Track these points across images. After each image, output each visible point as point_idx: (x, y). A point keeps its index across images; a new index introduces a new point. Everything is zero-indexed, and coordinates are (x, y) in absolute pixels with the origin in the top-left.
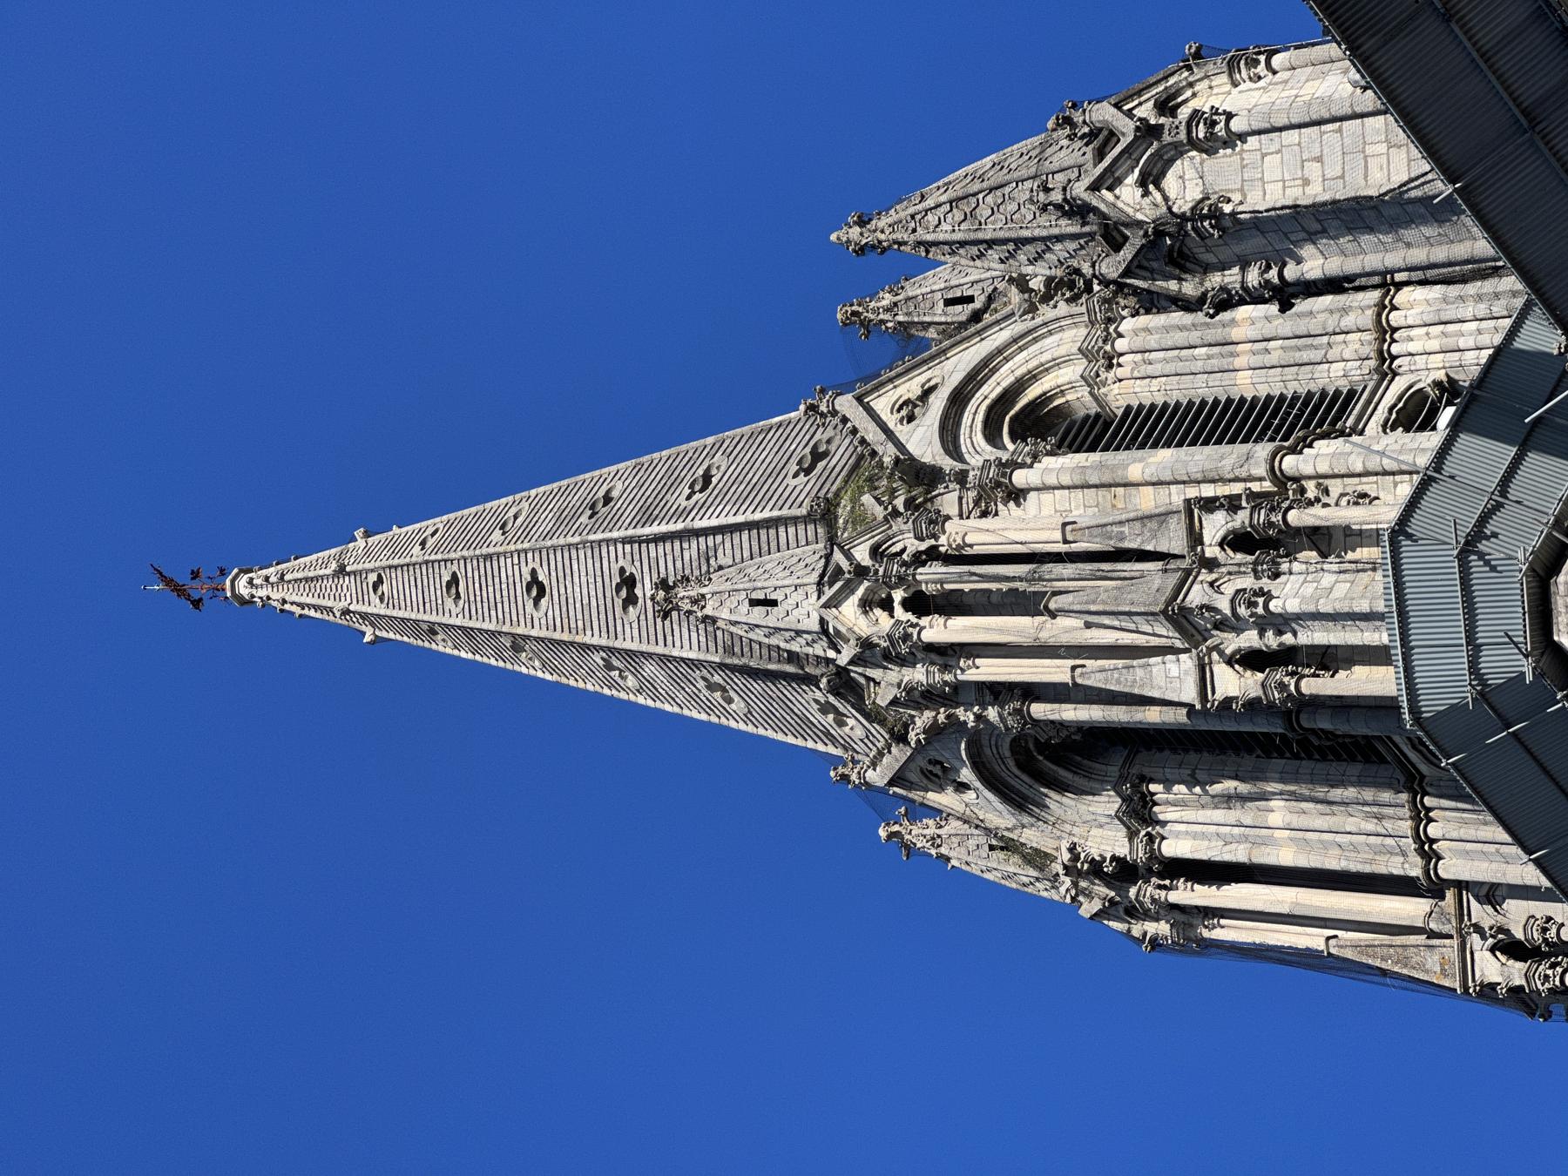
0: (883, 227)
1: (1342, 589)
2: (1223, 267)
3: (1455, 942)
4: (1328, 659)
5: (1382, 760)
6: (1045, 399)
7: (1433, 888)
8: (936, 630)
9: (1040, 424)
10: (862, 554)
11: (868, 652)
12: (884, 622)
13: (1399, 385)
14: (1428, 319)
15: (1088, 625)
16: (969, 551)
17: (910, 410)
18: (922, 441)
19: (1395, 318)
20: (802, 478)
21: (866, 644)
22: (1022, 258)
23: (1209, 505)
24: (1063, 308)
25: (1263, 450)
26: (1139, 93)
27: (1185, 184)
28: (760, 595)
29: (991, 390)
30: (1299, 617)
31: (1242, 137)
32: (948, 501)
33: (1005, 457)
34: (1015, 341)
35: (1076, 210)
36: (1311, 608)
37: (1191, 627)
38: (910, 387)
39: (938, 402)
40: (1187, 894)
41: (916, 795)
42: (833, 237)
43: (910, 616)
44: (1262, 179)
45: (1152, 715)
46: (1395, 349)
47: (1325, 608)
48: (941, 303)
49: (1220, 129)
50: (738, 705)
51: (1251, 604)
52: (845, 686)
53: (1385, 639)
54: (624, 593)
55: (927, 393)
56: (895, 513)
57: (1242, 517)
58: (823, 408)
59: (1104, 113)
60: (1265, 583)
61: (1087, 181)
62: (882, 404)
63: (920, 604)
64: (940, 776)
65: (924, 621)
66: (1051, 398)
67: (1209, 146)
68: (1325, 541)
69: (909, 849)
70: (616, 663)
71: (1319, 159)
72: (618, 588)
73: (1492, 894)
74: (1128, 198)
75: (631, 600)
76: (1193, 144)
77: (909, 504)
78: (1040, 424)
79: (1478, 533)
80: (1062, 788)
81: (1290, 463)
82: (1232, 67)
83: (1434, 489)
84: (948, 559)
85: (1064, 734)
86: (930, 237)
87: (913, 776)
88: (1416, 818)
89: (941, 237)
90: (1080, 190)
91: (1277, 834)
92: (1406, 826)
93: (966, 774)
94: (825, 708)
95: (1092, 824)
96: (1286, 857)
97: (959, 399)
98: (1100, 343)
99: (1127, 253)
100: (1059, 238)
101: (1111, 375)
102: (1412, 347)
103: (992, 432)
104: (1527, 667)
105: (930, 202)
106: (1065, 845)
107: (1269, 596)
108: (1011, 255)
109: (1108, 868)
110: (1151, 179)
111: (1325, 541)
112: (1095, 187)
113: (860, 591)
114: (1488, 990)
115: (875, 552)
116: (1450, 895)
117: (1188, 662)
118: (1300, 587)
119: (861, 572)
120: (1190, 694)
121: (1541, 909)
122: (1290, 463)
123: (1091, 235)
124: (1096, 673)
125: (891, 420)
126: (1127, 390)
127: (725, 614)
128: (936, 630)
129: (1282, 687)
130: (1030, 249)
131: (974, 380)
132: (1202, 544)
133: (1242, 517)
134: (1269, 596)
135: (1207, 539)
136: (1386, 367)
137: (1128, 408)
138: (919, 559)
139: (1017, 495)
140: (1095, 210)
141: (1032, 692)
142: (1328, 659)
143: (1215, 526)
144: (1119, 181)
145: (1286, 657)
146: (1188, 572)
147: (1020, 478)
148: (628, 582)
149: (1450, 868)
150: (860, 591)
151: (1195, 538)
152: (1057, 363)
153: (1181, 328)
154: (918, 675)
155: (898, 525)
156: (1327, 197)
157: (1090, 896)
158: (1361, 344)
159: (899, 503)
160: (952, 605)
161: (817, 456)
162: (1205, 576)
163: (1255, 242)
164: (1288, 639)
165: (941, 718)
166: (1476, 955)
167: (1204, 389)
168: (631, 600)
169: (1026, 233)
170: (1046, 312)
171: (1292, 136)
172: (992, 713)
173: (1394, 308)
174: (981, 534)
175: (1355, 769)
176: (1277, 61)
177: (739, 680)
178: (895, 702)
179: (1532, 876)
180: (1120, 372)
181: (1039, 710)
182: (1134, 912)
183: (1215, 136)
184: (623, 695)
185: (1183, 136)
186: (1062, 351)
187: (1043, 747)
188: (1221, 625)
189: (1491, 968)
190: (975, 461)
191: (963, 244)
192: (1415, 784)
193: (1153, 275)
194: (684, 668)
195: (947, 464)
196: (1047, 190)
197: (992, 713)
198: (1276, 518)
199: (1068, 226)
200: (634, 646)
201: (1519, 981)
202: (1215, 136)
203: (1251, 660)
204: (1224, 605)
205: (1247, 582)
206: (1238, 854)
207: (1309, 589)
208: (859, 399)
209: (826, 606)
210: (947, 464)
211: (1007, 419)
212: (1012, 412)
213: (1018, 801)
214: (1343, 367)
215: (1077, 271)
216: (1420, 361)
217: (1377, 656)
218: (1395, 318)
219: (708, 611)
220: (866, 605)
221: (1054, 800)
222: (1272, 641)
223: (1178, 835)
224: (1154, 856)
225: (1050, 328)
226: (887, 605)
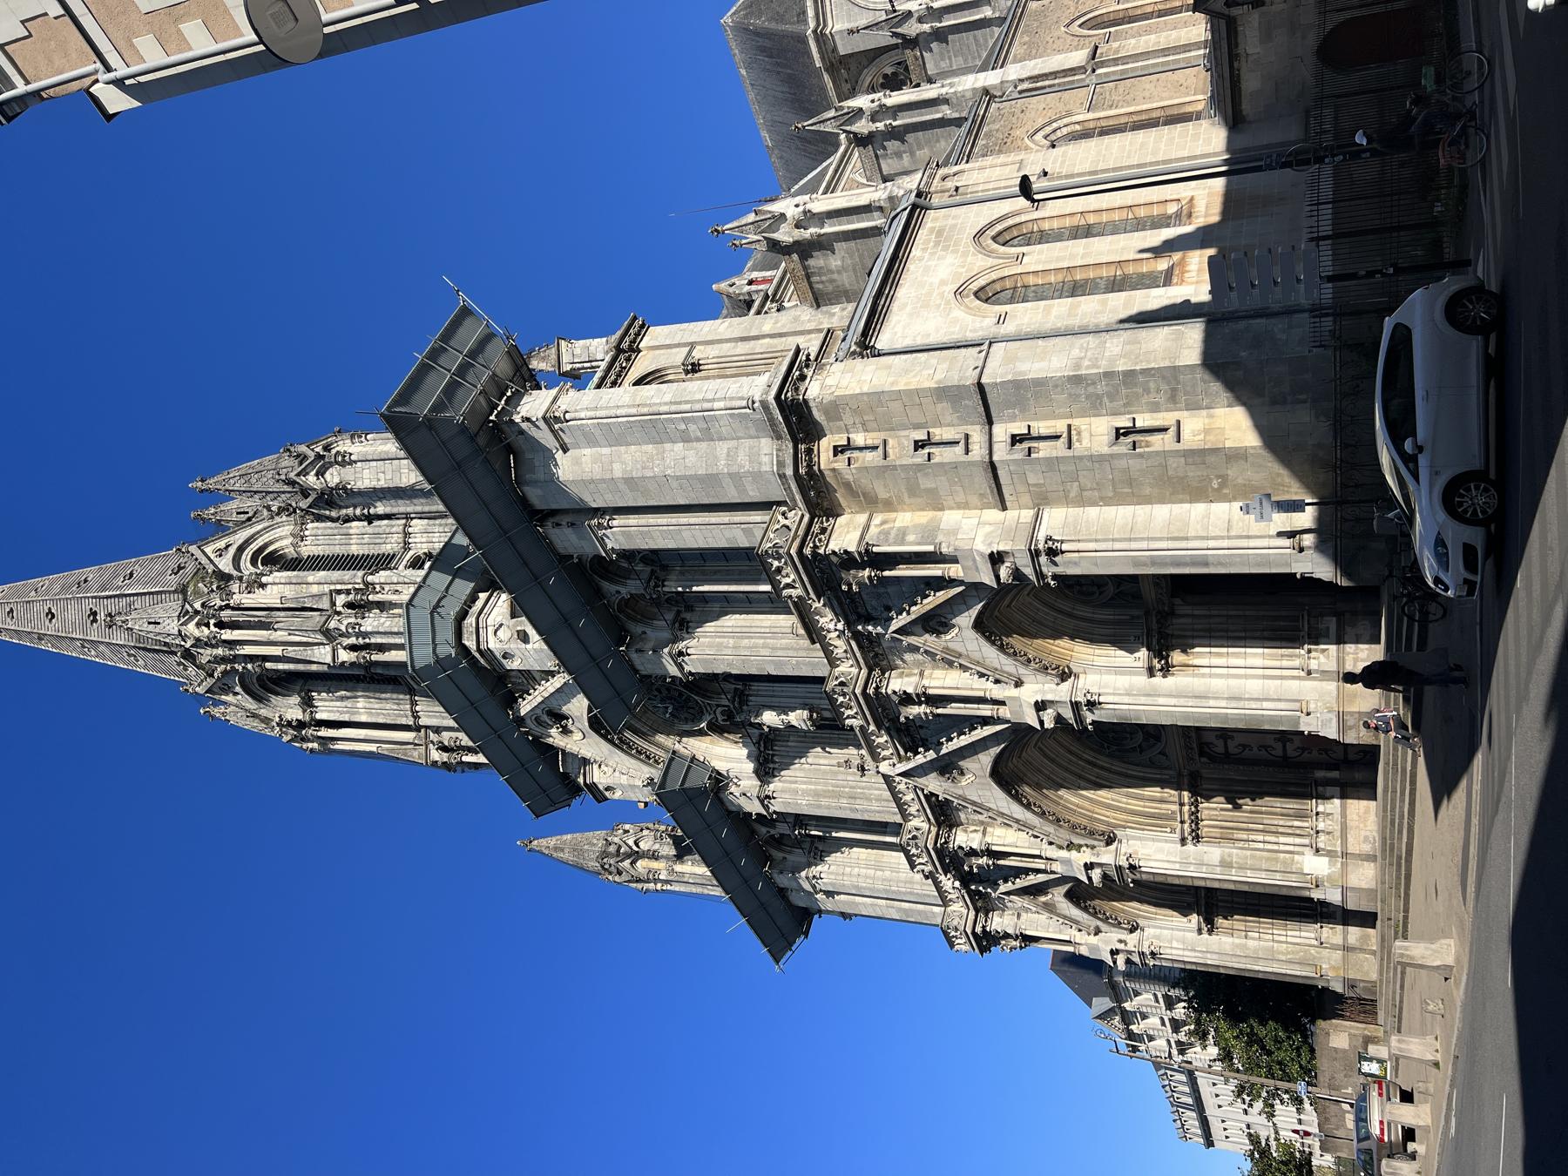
0: (211, 483)
4: (382, 648)
6: (275, 551)
7: (418, 728)
8: (227, 635)
9: (275, 560)
10: (197, 606)
11: (198, 642)
17: (220, 553)
18: (225, 564)
21: (198, 640)
23: (339, 592)
27: (333, 477)
29: (254, 547)
32: (235, 587)
35: (292, 483)
37: (330, 635)
38: (221, 544)
39: (232, 550)
40: (325, 732)
45: (314, 668)
55: (227, 547)
62: (209, 550)
63: (221, 625)
64: (227, 689)
67: (343, 464)
68: (382, 606)
74: (311, 479)
78: (275, 560)
79: (437, 606)
80: (277, 694)
81: (370, 579)
84: (233, 609)
90: (292, 475)
93: (238, 689)
96: (364, 719)
97: (241, 549)
103: (254, 562)
110: (320, 474)
111: (382, 606)
112: (298, 475)
115: (203, 605)
118: (371, 622)
119: (197, 612)
120: (329, 660)
121: (454, 734)
122: (370, 579)
124: (292, 652)
126: (307, 550)
128: (227, 635)
131: (247, 543)
136: (406, 546)
139: (263, 586)
141: (265, 658)
142: (382, 648)
143: (341, 600)
149: (423, 722)
151: (333, 604)
152: (281, 538)
160: (234, 626)
161: (180, 568)
170: (278, 519)
172: (249, 666)
174: (247, 600)
179: (452, 723)
181: (268, 665)
182: (304, 739)
183: (345, 461)
187: (270, 679)
189: (436, 755)
192: (412, 692)
195: (235, 573)
197: (249, 666)
199: (286, 488)
202: (345, 461)
203: (353, 648)
204: (343, 628)
205: (352, 620)
206: (346, 718)
210: (235, 573)
213: (258, 699)
220: (198, 625)
221: (273, 698)
224: (312, 719)
225: (279, 525)
226: (207, 625)
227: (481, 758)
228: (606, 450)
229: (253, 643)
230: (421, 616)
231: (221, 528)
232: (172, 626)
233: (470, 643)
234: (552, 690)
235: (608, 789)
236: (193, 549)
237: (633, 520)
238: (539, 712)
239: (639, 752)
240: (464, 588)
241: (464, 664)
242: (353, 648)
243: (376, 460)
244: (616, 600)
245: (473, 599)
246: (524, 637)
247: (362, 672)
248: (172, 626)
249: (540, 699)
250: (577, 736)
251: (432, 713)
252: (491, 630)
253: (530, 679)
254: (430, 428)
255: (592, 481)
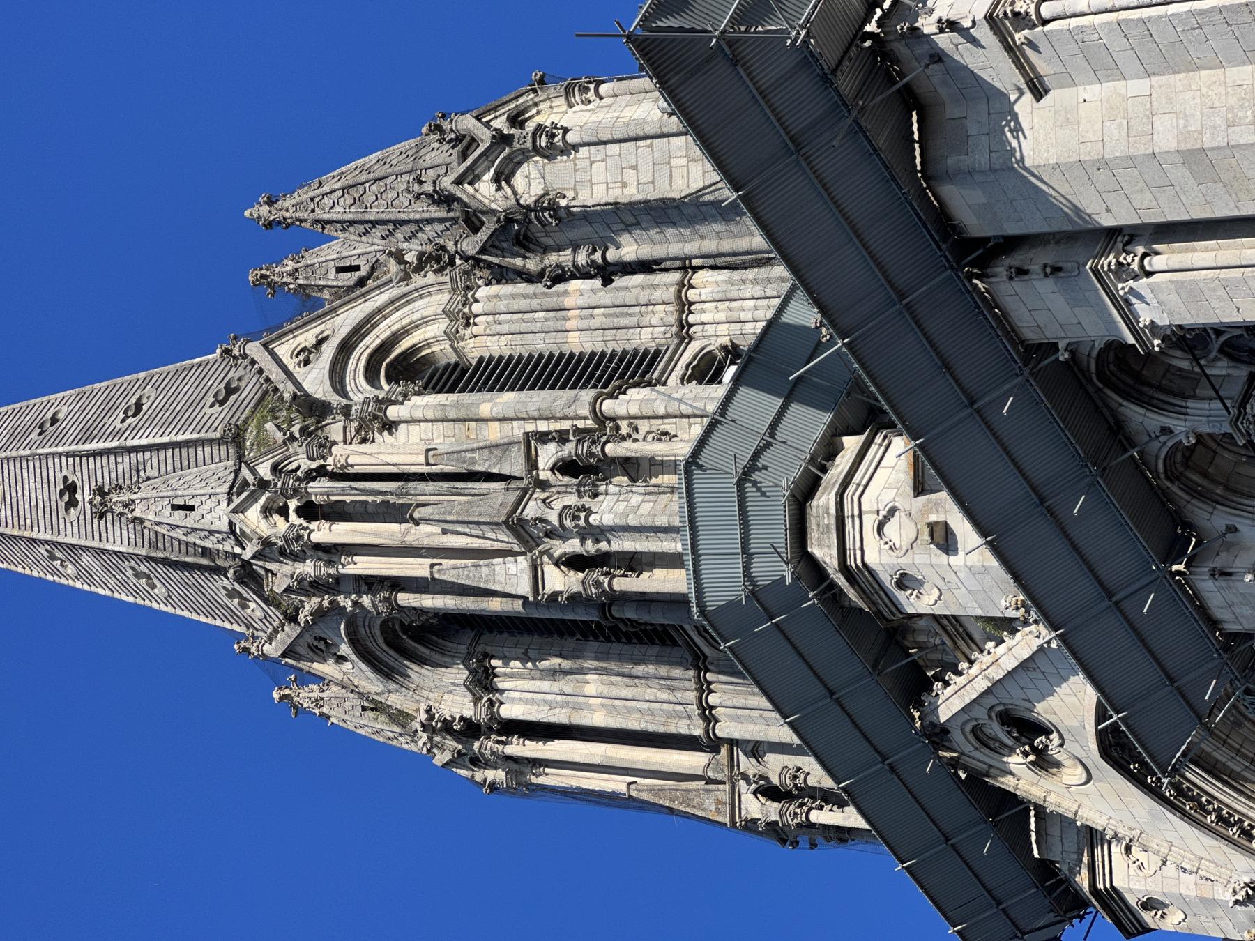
0: (288, 207)
1: (647, 507)
2: (559, 249)
3: (727, 787)
4: (635, 563)
5: (675, 644)
6: (414, 349)
7: (711, 744)
8: (323, 532)
10: (264, 470)
11: (267, 548)
12: (281, 525)
13: (694, 347)
14: (717, 297)
15: (445, 532)
16: (350, 470)
17: (306, 356)
18: (315, 381)
19: (692, 294)
20: (217, 408)
21: (266, 543)
22: (400, 236)
24: (431, 278)
25: (587, 395)
26: (495, 109)
27: (530, 182)
28: (180, 502)
29: (372, 341)
30: (613, 529)
31: (575, 147)
32: (335, 430)
33: (381, 395)
34: (392, 302)
35: (445, 200)
36: (622, 522)
38: (307, 338)
39: (329, 350)
40: (520, 748)
41: (303, 665)
42: (247, 213)
43: (302, 521)
45: (495, 605)
46: (691, 319)
47: (633, 521)
49: (558, 140)
50: (160, 590)
51: (575, 518)
52: (248, 576)
54: (66, 497)
55: (320, 342)
56: (292, 438)
57: (569, 448)
58: (236, 352)
59: (467, 123)
60: (586, 501)
61: (452, 176)
62: (284, 350)
63: (310, 511)
64: (323, 649)
65: (314, 525)
67: (550, 153)
68: (634, 468)
69: (297, 708)
70: (58, 554)
71: (635, 168)
72: (62, 493)
73: (756, 750)
74: (485, 191)
75: (72, 503)
76: (537, 151)
77: (303, 431)
80: (421, 661)
82: (568, 92)
83: (719, 430)
84: (334, 476)
85: (424, 618)
86: (325, 217)
87: (302, 650)
88: (700, 690)
89: (335, 217)
90: (447, 183)
91: (592, 701)
92: (692, 696)
93: (345, 649)
94: (232, 594)
95: (445, 691)
96: (598, 719)
97: (346, 348)
99: (483, 235)
100: (429, 221)
101: (468, 332)
102: (705, 317)
103: (371, 375)
104: (787, 572)
105: (326, 188)
106: (423, 707)
107: (589, 512)
108: (391, 233)
109: (457, 727)
110: (503, 177)
111: (634, 468)
112: (459, 182)
113: (262, 500)
114: (751, 824)
115: (275, 469)
116: (724, 750)
117: (523, 563)
118: (614, 505)
119: (263, 485)
120: (524, 588)
121: (792, 761)
122: (608, 406)
123: (455, 220)
124: (450, 570)
125: (291, 364)
126: (480, 345)
127: (151, 516)
128: (323, 532)
129: (598, 584)
130: (406, 229)
131: (358, 333)
133: (569, 448)
134: (589, 512)
135: (541, 465)
136: (684, 331)
137: (481, 359)
138: (311, 476)
139: (390, 426)
140: (459, 200)
141: (398, 584)
142: (635, 563)
143: (548, 455)
144: (478, 178)
145: (601, 561)
146: (525, 491)
147: (393, 412)
148: (71, 488)
149: (723, 730)
150: (262, 500)
151: (532, 464)
152: (425, 321)
153: (525, 296)
154: (307, 568)
155: (293, 447)
156: (640, 197)
157: (442, 749)
158: (664, 314)
159: (296, 430)
160: (336, 513)
161: (230, 391)
162: (539, 494)
163: (584, 230)
164: (603, 546)
165: (326, 603)
167: (541, 345)
168: (72, 503)
169: (403, 216)
170: (418, 280)
171: (614, 149)
172: (366, 600)
174: (361, 457)
175: (654, 650)
176: (603, 89)
177: (161, 569)
178: (288, 590)
179: (786, 735)
180: (475, 330)
181: (404, 599)
184: (63, 581)
185: (529, 145)
186: (430, 311)
187: (406, 629)
188: (550, 534)
189: (754, 807)
190: (357, 398)
191: (352, 223)
193: (503, 253)
194: (115, 560)
195: (335, 399)
196: (421, 182)
197: (366, 600)
198: (597, 449)
199: (437, 212)
200: (74, 541)
201: (774, 817)
202: (554, 145)
203: (575, 562)
204: (553, 518)
205: (572, 500)
206: (560, 717)
207: (621, 507)
208: (265, 346)
209: (234, 511)
210: (335, 399)
213: (386, 671)
214: (651, 333)
215: (443, 248)
216: (710, 329)
217: (671, 561)
218: (692, 294)
219: (137, 513)
220: (267, 511)
222: (591, 547)
223: (513, 701)
224: (493, 717)
225: (420, 292)
226: (284, 512)
227: (850, 818)
228: (1138, 86)
229: (374, 549)
230: (717, 490)
231: (307, 304)
232: (216, 515)
233: (824, 551)
234: (1009, 663)
235: (1149, 905)
236: (254, 349)
237: (1203, 253)
238: (981, 714)
239: (1224, 821)
240: (808, 424)
241: (812, 600)
242: (575, 562)
243: (620, 141)
244: (1159, 450)
245: (830, 450)
246: (944, 539)
247: (593, 616)
248: (216, 515)
249: (982, 685)
250: (1072, 774)
251: (744, 712)
252: (870, 522)
253: (959, 636)
254: (734, 62)
255: (1103, 164)
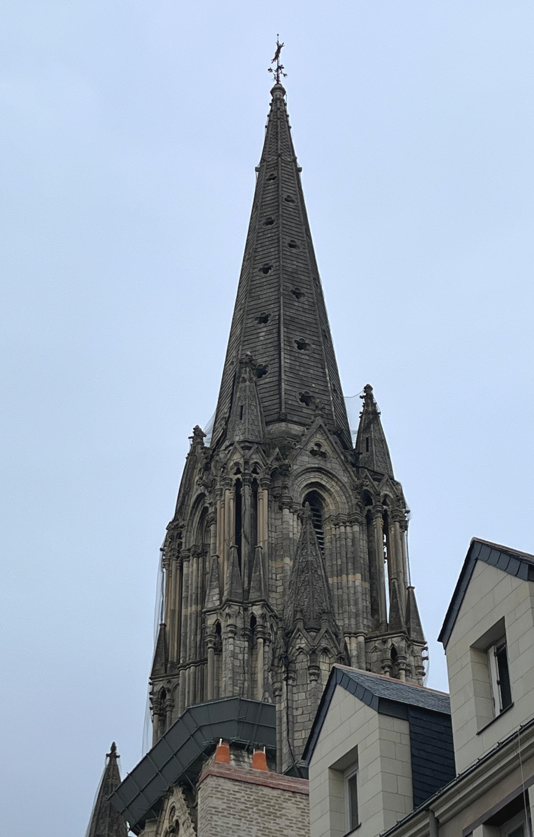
44: (299, 692)
48: (367, 436)
53: (209, 698)
66: (324, 502)
97: (319, 470)
98: (342, 521)
132: (252, 606)
166: (161, 682)
173: (350, 637)
211: (315, 489)
212: (317, 490)
